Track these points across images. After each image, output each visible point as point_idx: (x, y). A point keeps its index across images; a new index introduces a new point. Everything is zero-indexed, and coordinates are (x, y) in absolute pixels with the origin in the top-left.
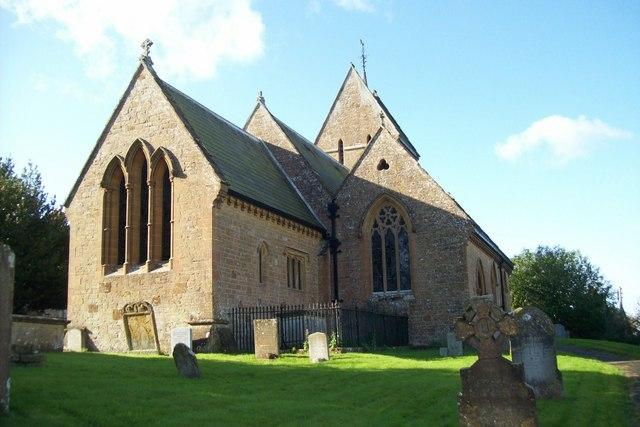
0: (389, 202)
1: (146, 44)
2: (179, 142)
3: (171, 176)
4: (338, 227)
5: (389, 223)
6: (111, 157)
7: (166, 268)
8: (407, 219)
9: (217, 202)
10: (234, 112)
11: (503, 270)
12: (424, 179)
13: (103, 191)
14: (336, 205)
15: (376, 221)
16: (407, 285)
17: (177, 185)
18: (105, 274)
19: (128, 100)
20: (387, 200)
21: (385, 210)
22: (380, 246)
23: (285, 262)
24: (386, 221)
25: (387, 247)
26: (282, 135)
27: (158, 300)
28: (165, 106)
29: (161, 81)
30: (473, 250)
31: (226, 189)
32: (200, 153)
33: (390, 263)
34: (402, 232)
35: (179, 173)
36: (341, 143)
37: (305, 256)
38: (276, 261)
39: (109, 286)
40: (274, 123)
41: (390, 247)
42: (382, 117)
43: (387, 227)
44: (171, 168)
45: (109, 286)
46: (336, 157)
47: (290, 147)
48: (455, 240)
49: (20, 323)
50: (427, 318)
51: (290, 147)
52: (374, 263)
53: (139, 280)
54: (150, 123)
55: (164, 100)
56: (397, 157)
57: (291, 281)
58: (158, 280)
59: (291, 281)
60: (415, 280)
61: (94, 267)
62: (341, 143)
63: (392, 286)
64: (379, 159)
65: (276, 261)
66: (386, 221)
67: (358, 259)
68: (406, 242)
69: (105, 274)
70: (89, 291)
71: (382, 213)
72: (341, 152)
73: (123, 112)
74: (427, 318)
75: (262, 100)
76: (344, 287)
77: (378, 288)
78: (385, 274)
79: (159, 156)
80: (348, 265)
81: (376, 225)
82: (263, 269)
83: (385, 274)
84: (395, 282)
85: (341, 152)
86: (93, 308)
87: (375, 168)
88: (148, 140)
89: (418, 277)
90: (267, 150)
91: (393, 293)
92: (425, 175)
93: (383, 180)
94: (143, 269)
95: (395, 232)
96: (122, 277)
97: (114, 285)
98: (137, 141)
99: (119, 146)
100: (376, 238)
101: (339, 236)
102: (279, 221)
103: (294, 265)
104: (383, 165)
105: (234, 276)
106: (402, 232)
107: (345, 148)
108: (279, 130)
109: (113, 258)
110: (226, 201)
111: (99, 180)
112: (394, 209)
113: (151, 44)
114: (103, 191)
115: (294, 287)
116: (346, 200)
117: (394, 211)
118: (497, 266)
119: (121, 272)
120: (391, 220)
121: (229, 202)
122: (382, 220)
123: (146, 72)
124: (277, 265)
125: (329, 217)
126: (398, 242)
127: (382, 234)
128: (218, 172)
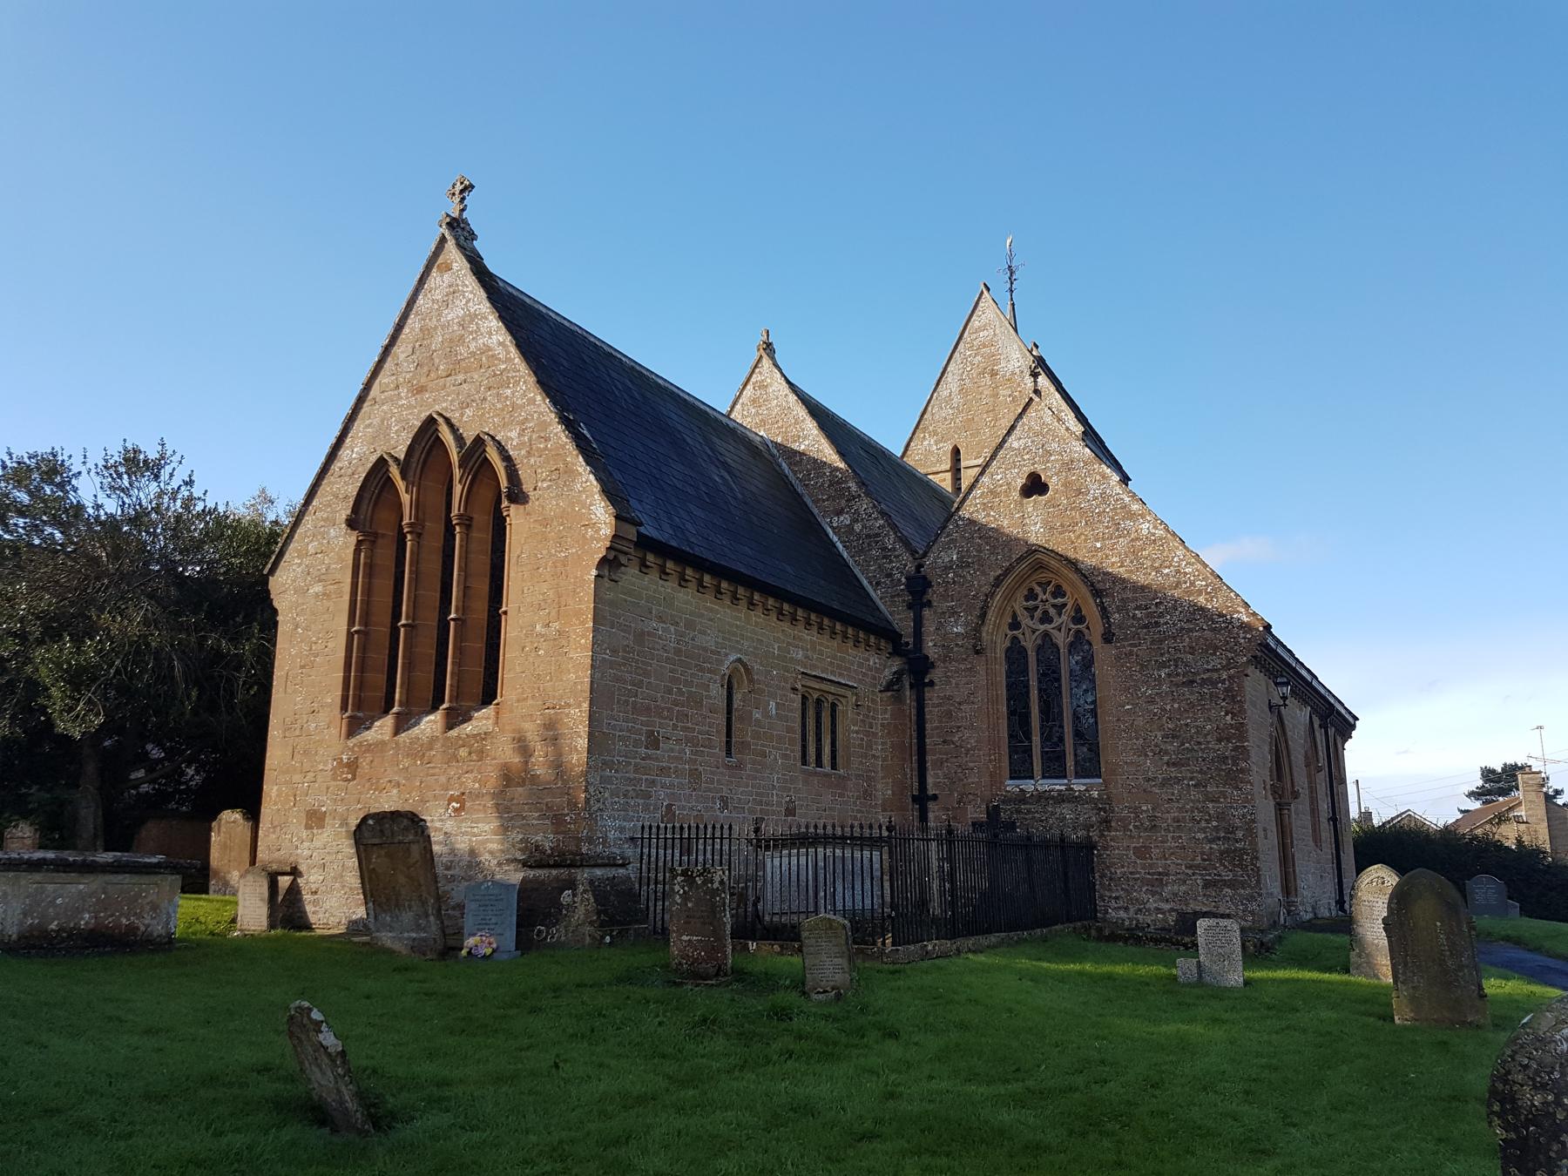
0: (1036, 568)
1: (459, 187)
2: (516, 414)
3: (505, 503)
4: (929, 627)
5: (1046, 618)
6: (373, 459)
7: (482, 720)
8: (1091, 610)
9: (609, 564)
10: (698, 359)
11: (1331, 731)
12: (1132, 516)
13: (352, 538)
14: (924, 578)
15: (1014, 616)
16: (1089, 769)
17: (515, 517)
18: (351, 733)
19: (413, 322)
20: (1040, 566)
21: (1038, 589)
22: (1025, 672)
23: (797, 704)
24: (1038, 614)
25: (1042, 677)
26: (811, 426)
27: (423, 801)
28: (494, 334)
29: (491, 275)
30: (1256, 685)
31: (631, 532)
32: (570, 447)
33: (1050, 711)
34: (1079, 642)
35: (518, 495)
36: (956, 452)
37: (849, 694)
38: (772, 704)
39: (352, 766)
40: (792, 398)
41: (1050, 676)
42: (1035, 375)
43: (1042, 627)
44: (504, 483)
45: (352, 766)
46: (945, 482)
47: (813, 442)
48: (1215, 662)
49: (38, 877)
50: (1142, 852)
51: (827, 453)
52: (1011, 713)
53: (419, 752)
54: (460, 377)
55: (493, 322)
56: (1068, 466)
57: (812, 750)
58: (463, 752)
59: (812, 750)
60: (1107, 758)
61: (323, 717)
62: (956, 452)
63: (1054, 768)
64: (1027, 470)
65: (772, 704)
66: (1038, 614)
67: (971, 700)
68: (1088, 663)
69: (351, 733)
70: (311, 775)
71: (1031, 595)
72: (956, 471)
73: (401, 350)
74: (1142, 852)
75: (769, 348)
76: (940, 764)
77: (1021, 770)
78: (1036, 739)
79: (475, 452)
80: (949, 714)
81: (1015, 625)
82: (736, 725)
83: (1036, 739)
84: (1061, 757)
85: (956, 471)
86: (315, 819)
87: (1016, 495)
88: (455, 417)
89: (1118, 751)
90: (770, 461)
91: (1058, 785)
92: (1135, 507)
93: (1032, 524)
94: (431, 723)
95: (1061, 639)
96: (382, 745)
97: (364, 764)
98: (430, 421)
99: (389, 432)
100: (1015, 654)
101: (931, 648)
102: (780, 613)
103: (819, 710)
104: (1035, 486)
105: (653, 742)
106: (1079, 642)
107: (963, 464)
108: (801, 412)
109: (371, 692)
110: (636, 561)
111: (344, 511)
112: (1058, 587)
113: (469, 188)
114: (352, 538)
115: (819, 763)
116: (947, 568)
117: (1059, 592)
118: (1317, 723)
119: (383, 727)
120: (1052, 611)
121: (643, 565)
122: (1031, 611)
123: (452, 252)
124: (774, 713)
125: (910, 607)
126: (1068, 664)
127: (1029, 643)
128: (611, 493)
